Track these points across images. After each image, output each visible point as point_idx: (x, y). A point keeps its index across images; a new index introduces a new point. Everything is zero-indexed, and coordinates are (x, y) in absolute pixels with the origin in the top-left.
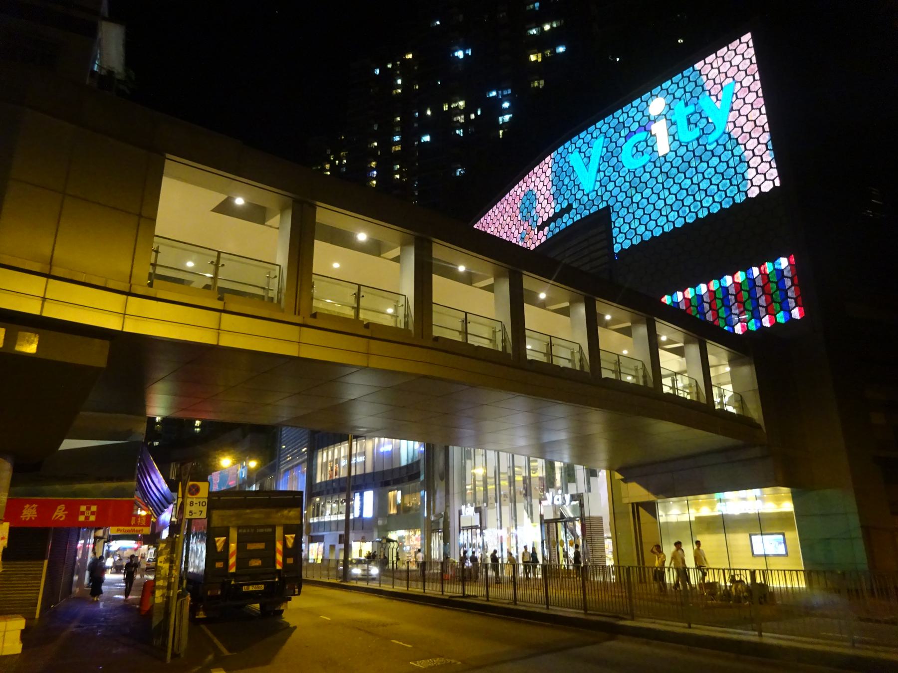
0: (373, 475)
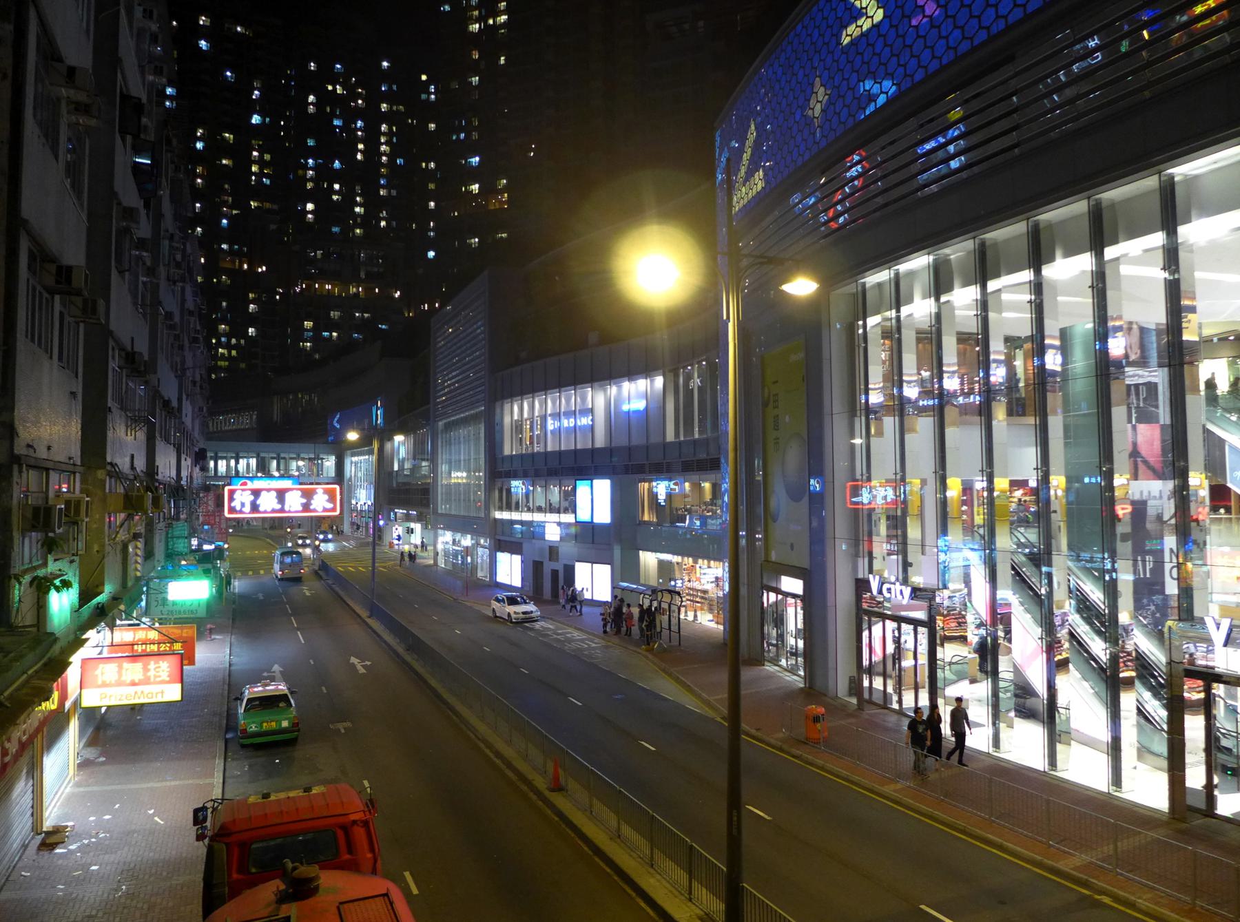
0: (609, 451)
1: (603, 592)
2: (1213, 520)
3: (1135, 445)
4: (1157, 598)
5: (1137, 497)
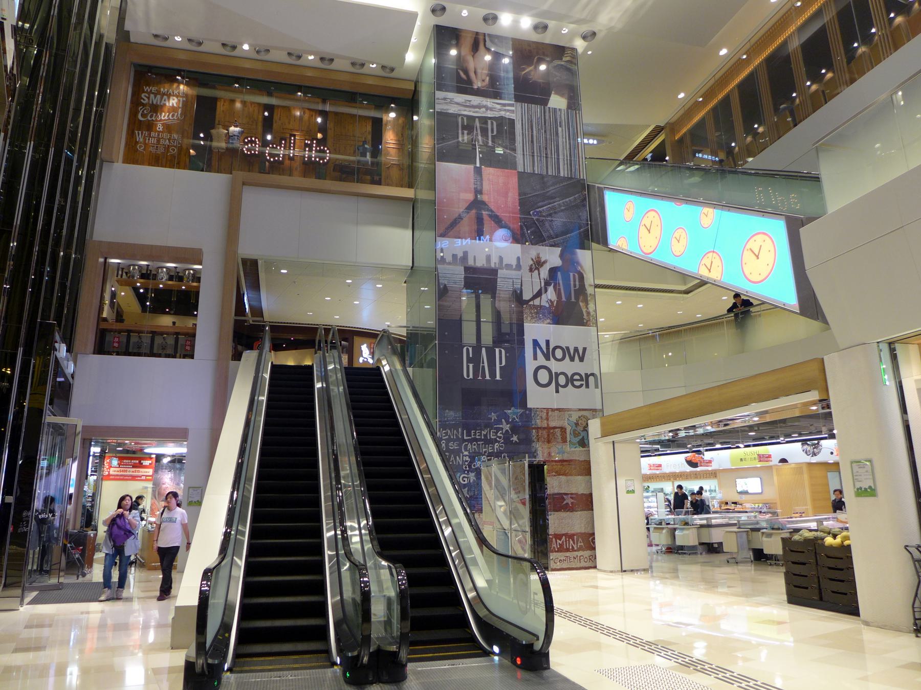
2: (195, 256)
4: (513, 413)
5: (481, 263)
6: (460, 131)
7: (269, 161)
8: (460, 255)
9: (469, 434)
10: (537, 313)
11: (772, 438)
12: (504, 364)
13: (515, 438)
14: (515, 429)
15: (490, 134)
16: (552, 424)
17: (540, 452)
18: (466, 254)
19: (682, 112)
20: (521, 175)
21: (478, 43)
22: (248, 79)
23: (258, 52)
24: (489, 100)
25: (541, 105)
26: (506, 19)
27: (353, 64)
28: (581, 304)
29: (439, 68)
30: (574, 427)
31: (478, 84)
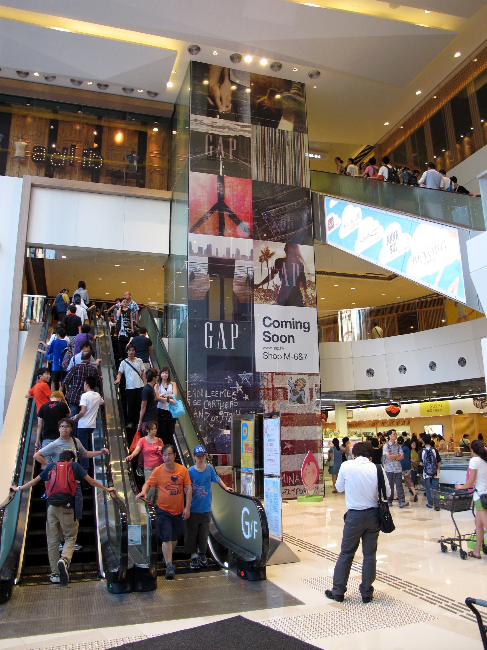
1: (242, 572)
3: (221, 198)
4: (244, 376)
5: (222, 254)
6: (207, 147)
7: (53, 166)
8: (205, 247)
9: (209, 394)
10: (265, 295)
11: (451, 395)
12: (237, 336)
13: (246, 397)
14: (246, 389)
15: (231, 150)
16: (276, 386)
17: (266, 409)
18: (209, 247)
19: (387, 137)
20: (256, 184)
21: (224, 75)
22: (37, 99)
23: (46, 78)
24: (231, 122)
25: (272, 127)
26: (248, 59)
27: (124, 89)
28: (301, 288)
29: (193, 95)
30: (294, 388)
31: (223, 109)
